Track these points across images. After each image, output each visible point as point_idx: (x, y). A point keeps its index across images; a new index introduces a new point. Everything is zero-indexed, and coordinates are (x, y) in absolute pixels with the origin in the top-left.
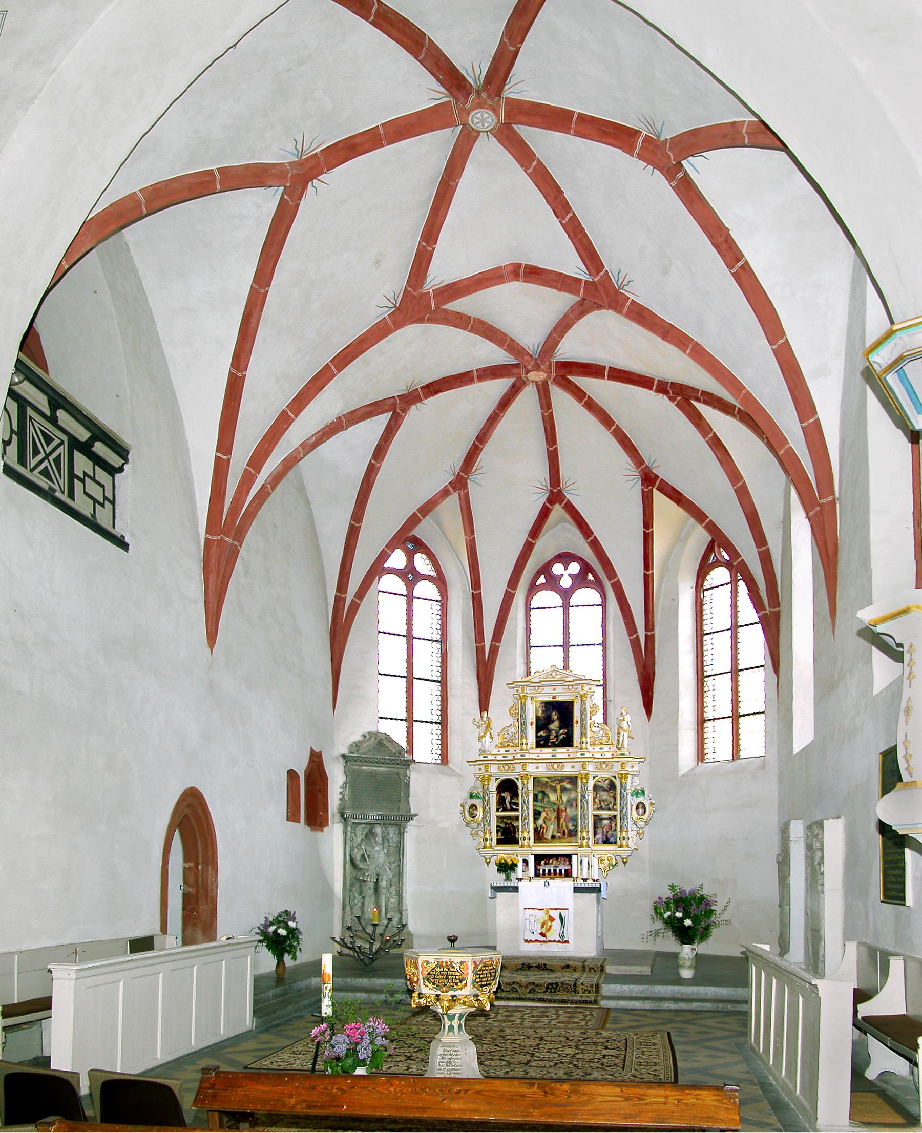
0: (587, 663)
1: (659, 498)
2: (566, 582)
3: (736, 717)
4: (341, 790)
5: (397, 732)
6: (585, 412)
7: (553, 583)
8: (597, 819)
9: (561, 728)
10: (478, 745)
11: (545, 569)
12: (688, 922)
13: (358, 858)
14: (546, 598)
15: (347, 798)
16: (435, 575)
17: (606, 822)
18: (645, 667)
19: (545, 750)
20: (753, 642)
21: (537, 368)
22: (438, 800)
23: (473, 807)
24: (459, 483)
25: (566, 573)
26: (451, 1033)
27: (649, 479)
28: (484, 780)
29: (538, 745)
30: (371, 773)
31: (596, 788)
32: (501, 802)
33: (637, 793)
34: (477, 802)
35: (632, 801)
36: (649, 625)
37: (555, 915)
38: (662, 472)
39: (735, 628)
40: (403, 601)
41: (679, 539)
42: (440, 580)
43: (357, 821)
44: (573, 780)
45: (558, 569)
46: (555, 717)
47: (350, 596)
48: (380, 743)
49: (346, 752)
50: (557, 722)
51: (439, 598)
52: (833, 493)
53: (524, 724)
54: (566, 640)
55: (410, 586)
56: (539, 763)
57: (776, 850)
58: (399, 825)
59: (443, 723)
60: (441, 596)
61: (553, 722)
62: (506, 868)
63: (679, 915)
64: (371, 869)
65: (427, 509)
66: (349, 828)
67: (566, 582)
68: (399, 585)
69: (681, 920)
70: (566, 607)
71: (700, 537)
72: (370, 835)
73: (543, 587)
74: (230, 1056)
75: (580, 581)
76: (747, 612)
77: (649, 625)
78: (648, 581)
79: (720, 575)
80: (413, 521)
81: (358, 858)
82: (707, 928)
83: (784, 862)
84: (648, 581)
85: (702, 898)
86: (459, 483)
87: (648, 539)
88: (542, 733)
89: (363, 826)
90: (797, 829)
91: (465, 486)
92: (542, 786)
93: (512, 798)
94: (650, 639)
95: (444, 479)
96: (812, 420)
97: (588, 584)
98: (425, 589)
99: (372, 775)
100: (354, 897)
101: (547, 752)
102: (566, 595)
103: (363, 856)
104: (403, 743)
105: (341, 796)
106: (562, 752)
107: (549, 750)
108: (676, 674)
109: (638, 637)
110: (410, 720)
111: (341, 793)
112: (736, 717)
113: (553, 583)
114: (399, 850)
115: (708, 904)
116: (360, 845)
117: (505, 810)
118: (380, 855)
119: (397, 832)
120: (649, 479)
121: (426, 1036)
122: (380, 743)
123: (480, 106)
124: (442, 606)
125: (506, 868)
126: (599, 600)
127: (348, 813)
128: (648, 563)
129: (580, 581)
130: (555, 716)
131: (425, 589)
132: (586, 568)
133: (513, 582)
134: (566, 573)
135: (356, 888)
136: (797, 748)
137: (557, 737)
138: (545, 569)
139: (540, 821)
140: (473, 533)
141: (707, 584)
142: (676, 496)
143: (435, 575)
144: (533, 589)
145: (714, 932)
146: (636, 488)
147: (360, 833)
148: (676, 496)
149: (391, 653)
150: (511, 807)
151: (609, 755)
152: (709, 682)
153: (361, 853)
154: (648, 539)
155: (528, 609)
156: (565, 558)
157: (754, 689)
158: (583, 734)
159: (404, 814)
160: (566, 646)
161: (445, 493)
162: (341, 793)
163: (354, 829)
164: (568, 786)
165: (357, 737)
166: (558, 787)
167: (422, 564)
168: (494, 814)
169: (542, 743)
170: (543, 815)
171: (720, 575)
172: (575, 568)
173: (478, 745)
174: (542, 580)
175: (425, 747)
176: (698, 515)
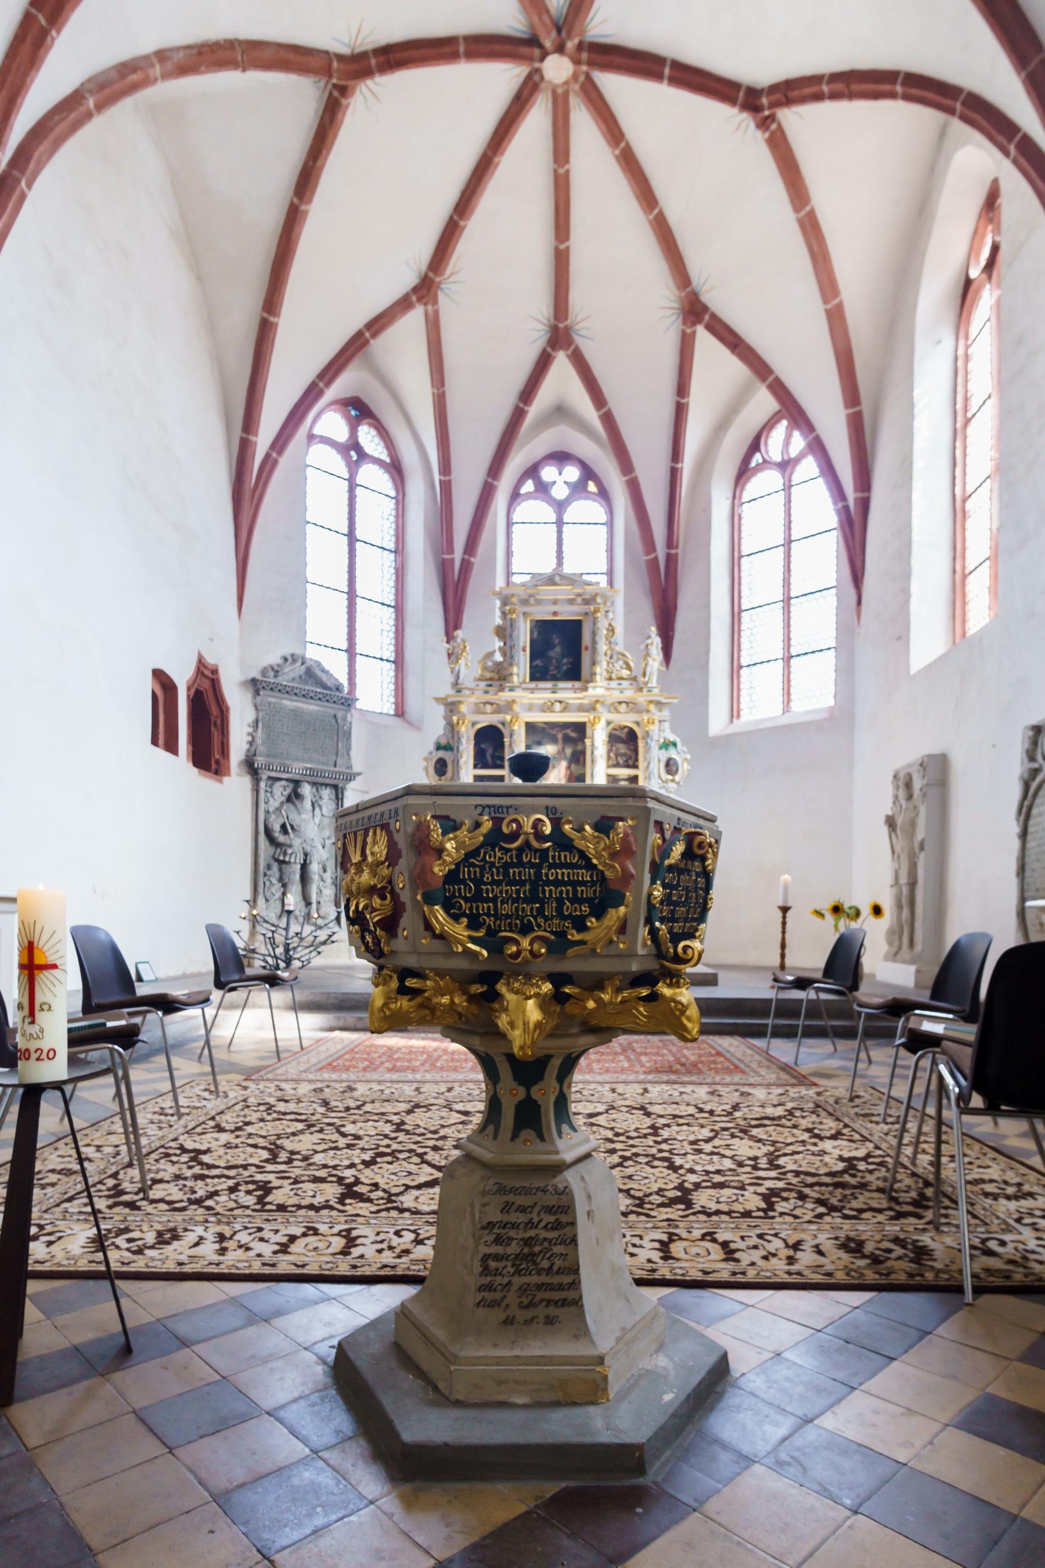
2: (560, 492)
4: (251, 730)
5: (336, 667)
9: (563, 656)
13: (277, 827)
14: (533, 511)
15: (259, 741)
16: (388, 460)
26: (528, 1133)
27: (694, 310)
30: (295, 711)
42: (396, 469)
43: (273, 774)
45: (548, 473)
46: (557, 641)
47: (263, 440)
50: (561, 649)
51: (393, 494)
55: (353, 468)
61: (554, 647)
65: (378, 324)
66: (262, 784)
67: (560, 492)
68: (337, 463)
70: (560, 523)
72: (294, 797)
73: (529, 496)
75: (578, 489)
81: (277, 827)
86: (425, 290)
88: (538, 662)
89: (284, 783)
93: (495, 750)
95: (406, 279)
96: (1035, 62)
98: (373, 476)
99: (296, 714)
100: (271, 883)
102: (560, 507)
103: (283, 827)
105: (250, 738)
109: (656, 558)
110: (351, 651)
111: (249, 734)
113: (543, 489)
116: (278, 810)
117: (485, 766)
119: (333, 797)
120: (694, 310)
121: (388, 1108)
124: (397, 504)
126: (604, 518)
127: (260, 761)
132: (588, 473)
133: (496, 468)
134: (561, 479)
137: (558, 668)
138: (532, 471)
140: (443, 385)
141: (746, 496)
143: (388, 460)
144: (515, 496)
147: (280, 791)
150: (494, 762)
153: (281, 821)
155: (509, 524)
156: (561, 458)
159: (343, 770)
161: (403, 304)
162: (249, 734)
164: (573, 735)
166: (560, 736)
167: (367, 437)
172: (572, 473)
175: (374, 692)
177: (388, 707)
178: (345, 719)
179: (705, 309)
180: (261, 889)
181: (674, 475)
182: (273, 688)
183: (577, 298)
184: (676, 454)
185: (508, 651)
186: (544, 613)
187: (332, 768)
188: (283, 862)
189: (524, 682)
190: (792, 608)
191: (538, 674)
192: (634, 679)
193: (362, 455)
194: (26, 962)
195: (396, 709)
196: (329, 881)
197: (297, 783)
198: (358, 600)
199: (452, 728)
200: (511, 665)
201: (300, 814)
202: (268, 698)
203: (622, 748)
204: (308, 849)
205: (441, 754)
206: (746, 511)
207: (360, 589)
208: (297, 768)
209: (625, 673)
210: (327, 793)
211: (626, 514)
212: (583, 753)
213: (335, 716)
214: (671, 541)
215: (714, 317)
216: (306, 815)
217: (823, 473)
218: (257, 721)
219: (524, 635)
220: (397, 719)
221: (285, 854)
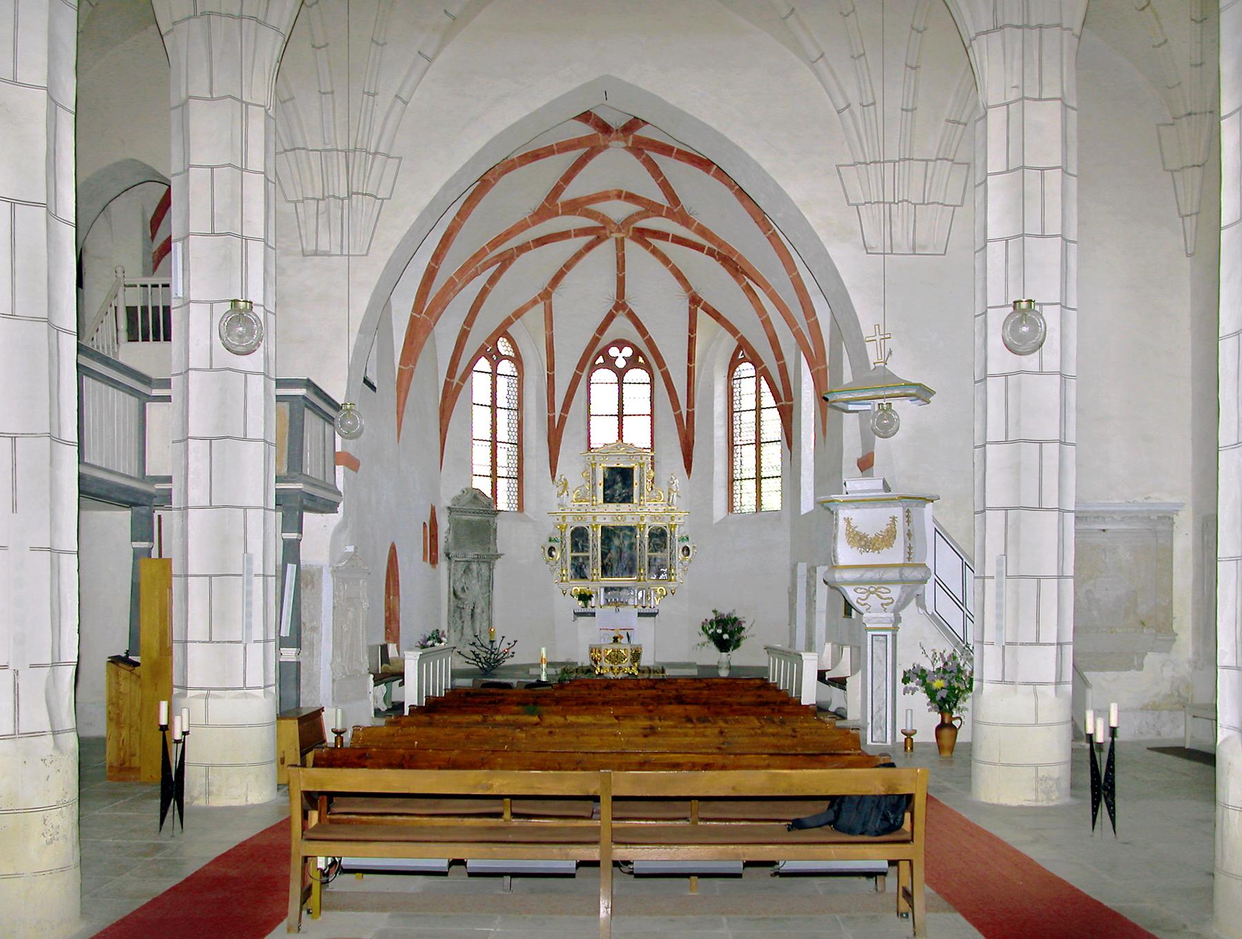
0: (638, 433)
1: (701, 315)
2: (621, 363)
3: (759, 479)
5: (484, 485)
6: (650, 256)
7: (610, 363)
10: (558, 501)
11: (604, 352)
12: (726, 636)
14: (604, 376)
18: (686, 437)
20: (772, 424)
21: (619, 230)
22: (519, 543)
23: (552, 549)
24: (546, 295)
25: (621, 356)
27: (695, 300)
28: (562, 529)
29: (605, 501)
31: (651, 535)
32: (575, 546)
33: (682, 539)
35: (679, 546)
36: (690, 404)
37: (624, 634)
38: (705, 297)
40: (488, 377)
42: (517, 360)
44: (632, 529)
45: (614, 352)
48: (475, 497)
49: (450, 505)
50: (619, 483)
52: (825, 363)
53: (594, 485)
54: (620, 414)
55: (494, 365)
57: (788, 584)
58: (489, 563)
59: (520, 478)
62: (585, 597)
63: (719, 631)
64: (469, 598)
65: (518, 314)
67: (621, 363)
69: (721, 635)
70: (620, 383)
72: (467, 570)
73: (601, 366)
75: (632, 363)
76: (768, 399)
77: (690, 404)
78: (690, 372)
79: (746, 369)
80: (509, 322)
82: (739, 640)
83: (793, 593)
84: (690, 372)
85: (736, 619)
86: (546, 295)
87: (691, 341)
90: (802, 569)
91: (550, 297)
92: (608, 533)
94: (690, 415)
97: (639, 366)
98: (505, 367)
99: (469, 523)
101: (612, 507)
102: (621, 374)
103: (463, 589)
106: (624, 507)
112: (759, 479)
113: (610, 363)
114: (490, 583)
115: (740, 623)
116: (460, 580)
117: (578, 551)
118: (476, 587)
120: (695, 300)
122: (475, 497)
123: (618, 139)
125: (585, 597)
127: (453, 553)
128: (691, 359)
129: (632, 363)
130: (618, 478)
131: (505, 367)
132: (637, 353)
134: (621, 356)
135: (457, 615)
136: (804, 511)
139: (606, 561)
142: (716, 316)
144: (594, 368)
145: (743, 642)
146: (683, 305)
147: (461, 568)
148: (716, 316)
149: (481, 419)
151: (661, 509)
152: (738, 449)
154: (691, 341)
155: (589, 384)
156: (621, 344)
157: (773, 456)
158: (641, 494)
160: (620, 415)
161: (535, 302)
165: (458, 492)
168: (569, 555)
169: (607, 499)
171: (746, 369)
172: (628, 352)
173: (558, 501)
174: (600, 360)
176: (733, 331)
177: (515, 508)
194: (114, 700)
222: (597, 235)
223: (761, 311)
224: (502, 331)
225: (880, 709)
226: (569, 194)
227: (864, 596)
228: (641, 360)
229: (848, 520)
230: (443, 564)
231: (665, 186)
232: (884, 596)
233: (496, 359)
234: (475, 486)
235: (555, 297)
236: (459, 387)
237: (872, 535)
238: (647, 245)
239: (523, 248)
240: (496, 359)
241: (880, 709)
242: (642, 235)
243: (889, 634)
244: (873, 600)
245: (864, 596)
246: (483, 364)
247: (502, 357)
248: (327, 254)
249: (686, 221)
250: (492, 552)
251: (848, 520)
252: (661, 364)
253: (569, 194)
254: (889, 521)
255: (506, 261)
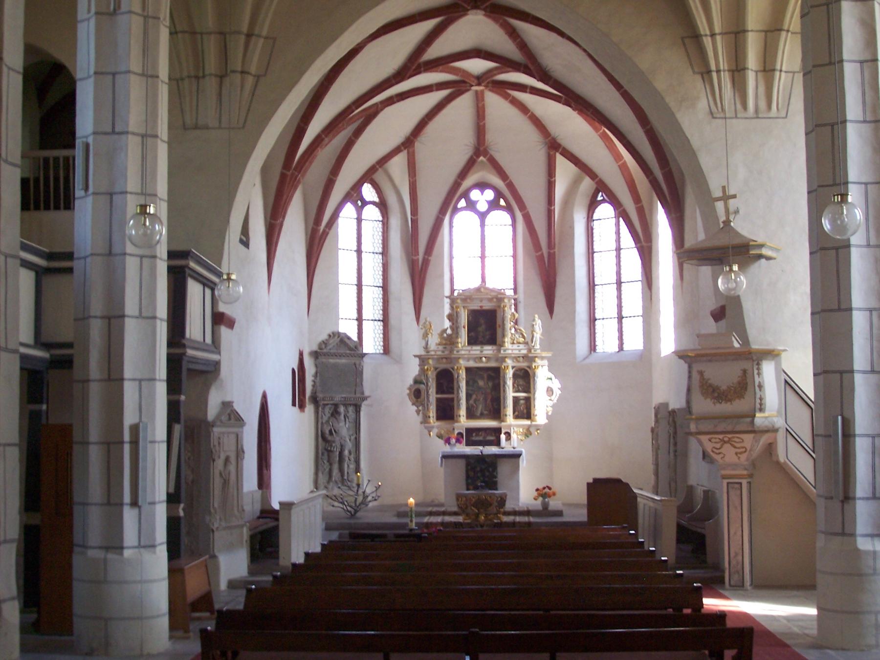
1: (560, 160)
2: (482, 207)
5: (349, 329)
7: (471, 206)
8: (516, 400)
15: (318, 384)
17: (522, 402)
19: (475, 348)
21: (479, 84)
34: (422, 387)
39: (618, 249)
41: (575, 184)
42: (383, 206)
45: (475, 194)
50: (485, 323)
55: (359, 210)
56: (469, 355)
60: (383, 217)
67: (482, 207)
71: (587, 184)
73: (462, 209)
74: (733, 339)
75: (494, 205)
76: (627, 239)
79: (605, 211)
81: (327, 432)
88: (472, 334)
98: (372, 213)
101: (476, 350)
102: (483, 216)
103: (330, 432)
104: (354, 337)
107: (478, 348)
108: (573, 283)
109: (542, 254)
113: (471, 206)
116: (328, 422)
117: (443, 392)
126: (510, 221)
127: (320, 395)
129: (494, 205)
130: (482, 321)
132: (499, 194)
134: (482, 198)
139: (471, 402)
141: (595, 216)
146: (540, 154)
147: (328, 411)
156: (482, 186)
157: (633, 294)
161: (396, 151)
163: (323, 409)
165: (324, 337)
166: (485, 376)
170: (474, 396)
171: (605, 211)
172: (489, 194)
175: (372, 344)
177: (381, 350)
178: (360, 364)
179: (559, 145)
180: (320, 467)
181: (550, 213)
182: (325, 354)
183: (480, 264)
184: (550, 200)
185: (455, 327)
186: (475, 306)
187: (353, 396)
188: (331, 451)
189: (465, 345)
190: (623, 288)
191: (472, 341)
192: (526, 343)
193: (365, 203)
195: (384, 350)
196: (352, 459)
197: (336, 406)
198: (364, 287)
199: (423, 371)
200: (457, 337)
201: (339, 423)
202: (322, 359)
203: (521, 382)
204: (343, 442)
205: (417, 386)
206: (596, 225)
207: (354, 255)
208: (338, 398)
209: (522, 340)
210: (351, 409)
211: (524, 234)
212: (499, 384)
213: (355, 364)
214: (551, 245)
215: (564, 149)
216: (342, 424)
217: (594, 285)
218: (316, 373)
219: (464, 320)
220: (385, 357)
221: (331, 446)
222: (458, 87)
223: (618, 157)
224: (368, 176)
225: (736, 554)
226: (435, 51)
227: (718, 446)
228: (502, 202)
229: (701, 373)
230: (310, 408)
231: (523, 46)
232: (738, 445)
233: (361, 204)
234: (341, 330)
235: (418, 145)
236: (325, 234)
237: (724, 387)
238: (506, 97)
239: (390, 101)
240: (361, 204)
241: (736, 554)
242: (502, 88)
243: (744, 482)
244: (728, 450)
245: (718, 446)
246: (349, 210)
247: (365, 203)
248: (206, 127)
249: (544, 75)
250: (358, 395)
251: (701, 373)
252: (522, 206)
253: (435, 51)
254: (740, 373)
255: (371, 116)
